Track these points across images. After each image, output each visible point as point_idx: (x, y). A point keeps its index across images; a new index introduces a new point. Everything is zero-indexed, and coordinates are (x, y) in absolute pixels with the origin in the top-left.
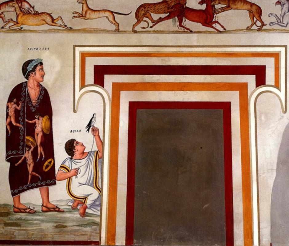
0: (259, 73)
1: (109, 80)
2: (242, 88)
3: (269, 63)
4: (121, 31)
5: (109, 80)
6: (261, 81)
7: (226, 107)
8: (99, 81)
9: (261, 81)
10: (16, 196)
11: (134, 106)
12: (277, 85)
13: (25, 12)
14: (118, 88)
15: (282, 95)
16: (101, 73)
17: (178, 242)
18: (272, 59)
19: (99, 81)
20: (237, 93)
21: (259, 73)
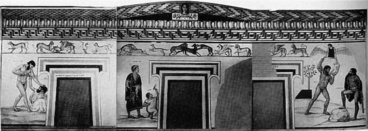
0: (100, 68)
1: (161, 72)
2: (206, 75)
6: (294, 74)
7: (169, 81)
8: (158, 73)
9: (294, 74)
11: (169, 81)
14: (164, 75)
15: (301, 77)
16: (158, 70)
19: (158, 73)
21: (211, 70)
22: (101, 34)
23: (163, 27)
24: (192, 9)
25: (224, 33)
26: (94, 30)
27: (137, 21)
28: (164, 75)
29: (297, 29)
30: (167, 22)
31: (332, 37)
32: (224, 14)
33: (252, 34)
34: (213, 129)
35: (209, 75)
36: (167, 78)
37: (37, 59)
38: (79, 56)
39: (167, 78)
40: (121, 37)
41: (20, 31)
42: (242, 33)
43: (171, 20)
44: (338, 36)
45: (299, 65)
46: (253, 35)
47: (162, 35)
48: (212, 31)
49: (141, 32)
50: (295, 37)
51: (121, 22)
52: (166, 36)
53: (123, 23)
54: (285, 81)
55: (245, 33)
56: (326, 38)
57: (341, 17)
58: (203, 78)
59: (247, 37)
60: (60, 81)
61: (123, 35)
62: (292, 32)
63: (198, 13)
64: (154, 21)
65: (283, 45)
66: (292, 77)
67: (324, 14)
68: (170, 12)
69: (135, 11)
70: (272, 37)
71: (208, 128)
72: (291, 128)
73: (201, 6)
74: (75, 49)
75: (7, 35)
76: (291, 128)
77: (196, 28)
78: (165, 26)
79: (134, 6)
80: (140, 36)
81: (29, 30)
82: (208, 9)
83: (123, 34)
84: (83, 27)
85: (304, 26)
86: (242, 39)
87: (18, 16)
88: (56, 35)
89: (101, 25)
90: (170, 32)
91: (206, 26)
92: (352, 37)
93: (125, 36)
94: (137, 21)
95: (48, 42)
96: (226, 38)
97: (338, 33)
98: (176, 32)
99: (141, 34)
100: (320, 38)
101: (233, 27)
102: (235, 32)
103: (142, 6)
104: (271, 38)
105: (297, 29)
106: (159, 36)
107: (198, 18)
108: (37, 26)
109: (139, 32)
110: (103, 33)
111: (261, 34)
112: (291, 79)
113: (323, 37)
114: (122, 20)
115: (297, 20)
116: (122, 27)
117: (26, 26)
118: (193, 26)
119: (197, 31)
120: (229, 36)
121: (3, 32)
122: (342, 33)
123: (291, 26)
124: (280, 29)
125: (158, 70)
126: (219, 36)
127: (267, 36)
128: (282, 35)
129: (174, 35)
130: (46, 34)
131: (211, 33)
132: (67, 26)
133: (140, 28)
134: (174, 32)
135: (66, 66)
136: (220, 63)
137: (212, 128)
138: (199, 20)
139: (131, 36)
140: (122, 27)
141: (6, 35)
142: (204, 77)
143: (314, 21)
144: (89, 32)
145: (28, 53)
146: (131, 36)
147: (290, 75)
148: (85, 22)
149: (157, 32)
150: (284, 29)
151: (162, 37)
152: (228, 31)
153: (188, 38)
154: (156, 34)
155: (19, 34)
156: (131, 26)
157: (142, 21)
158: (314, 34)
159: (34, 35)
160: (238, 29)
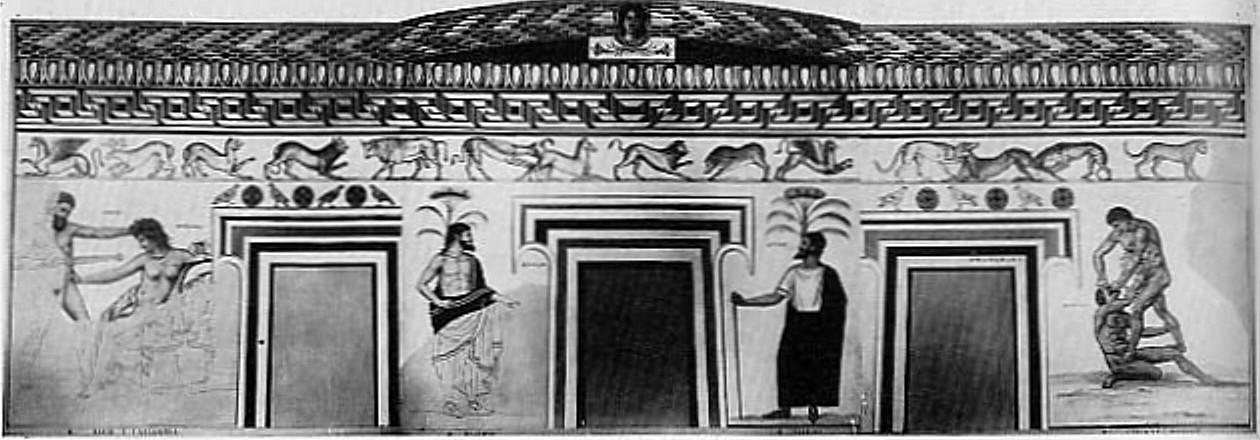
1: (554, 235)
2: (704, 245)
3: (533, 215)
4: (15, 138)
5: (554, 235)
6: (725, 238)
7: (583, 267)
8: (541, 236)
9: (725, 238)
10: (878, 405)
11: (583, 267)
12: (743, 243)
13: (1019, 74)
14: (563, 244)
15: (748, 251)
16: (542, 228)
17: (642, 399)
18: (737, 212)
19: (541, 236)
20: (1024, 257)
21: (723, 227)
22: (179, 111)
23: (501, 85)
24: (655, 22)
25: (653, 104)
26: (99, 97)
27: (531, 68)
28: (563, 244)
29: (1013, 89)
30: (492, 68)
31: (682, 116)
32: (811, 44)
33: (806, 105)
34: (731, 430)
35: (715, 245)
36: (575, 256)
37: (749, 194)
38: (740, 190)
39: (575, 256)
40: (417, 121)
41: (107, 109)
42: (717, 104)
43: (586, 59)
44: (759, 115)
45: (742, 208)
46: (753, 107)
47: (554, 113)
48: (783, 100)
49: (596, 104)
50: (891, 118)
51: (419, 68)
52: (510, 117)
53: (424, 74)
54: (583, 259)
55: (727, 104)
56: (998, 120)
57: (1160, 45)
58: (826, 259)
59: (1070, 116)
60: (588, 272)
61: (423, 112)
62: (826, 102)
63: (676, 36)
64: (469, 65)
65: (82, 142)
66: (719, 250)
67: (1103, 34)
68: (584, 34)
69: (59, 44)
70: (703, 116)
71: (718, 425)
72: (1035, 424)
73: (687, 13)
74: (1109, 165)
75: (314, 116)
76: (1035, 424)
77: (730, 90)
78: (546, 82)
79: (462, 14)
80: (539, 115)
81: (389, 100)
82: (712, 24)
83: (425, 109)
84: (170, 87)
85: (824, 79)
86: (1111, 123)
87: (173, 51)
88: (26, 112)
89: (580, 84)
90: (524, 102)
91: (972, 80)
92: (1147, 115)
93: (433, 116)
94: (531, 68)
95: (218, 142)
96: (886, 122)
97: (1155, 100)
98: (432, 102)
99: (483, 110)
100: (699, 121)
101: (1026, 82)
102: (691, 100)
103: (490, 16)
104: (981, 120)
105: (1127, 88)
106: (603, 117)
107: (677, 55)
108: (191, 83)
109: (590, 104)
110: (298, 109)
111: (1003, 106)
112: (712, 257)
113: (874, 116)
114: (423, 60)
115: (1014, 59)
116: (423, 88)
117: (95, 84)
118: (928, 82)
119: (843, 98)
120: (670, 113)
121: (20, 104)
122: (482, 104)
123: (991, 78)
124: (1069, 89)
125: (542, 228)
126: (1146, 111)
127: (685, 112)
128: (1020, 109)
129: (539, 111)
130: (217, 114)
131: (779, 105)
132: (462, 84)
133: (541, 89)
134: (424, 99)
135: (614, 224)
136: (753, 203)
137: (729, 426)
138: (678, 60)
139: (451, 116)
140: (423, 88)
141: (366, 115)
142: (699, 250)
143: (1068, 59)
144: (194, 103)
145: (396, 179)
146: (451, 116)
147: (707, 242)
148: (100, 70)
149: (540, 104)
150: (854, 90)
151: (155, 122)
152: (722, 97)
153: (1207, 119)
154: (533, 108)
155: (187, 114)
156: (451, 85)
157: (547, 66)
158: (735, 110)
159: (181, 115)
160: (812, 92)
